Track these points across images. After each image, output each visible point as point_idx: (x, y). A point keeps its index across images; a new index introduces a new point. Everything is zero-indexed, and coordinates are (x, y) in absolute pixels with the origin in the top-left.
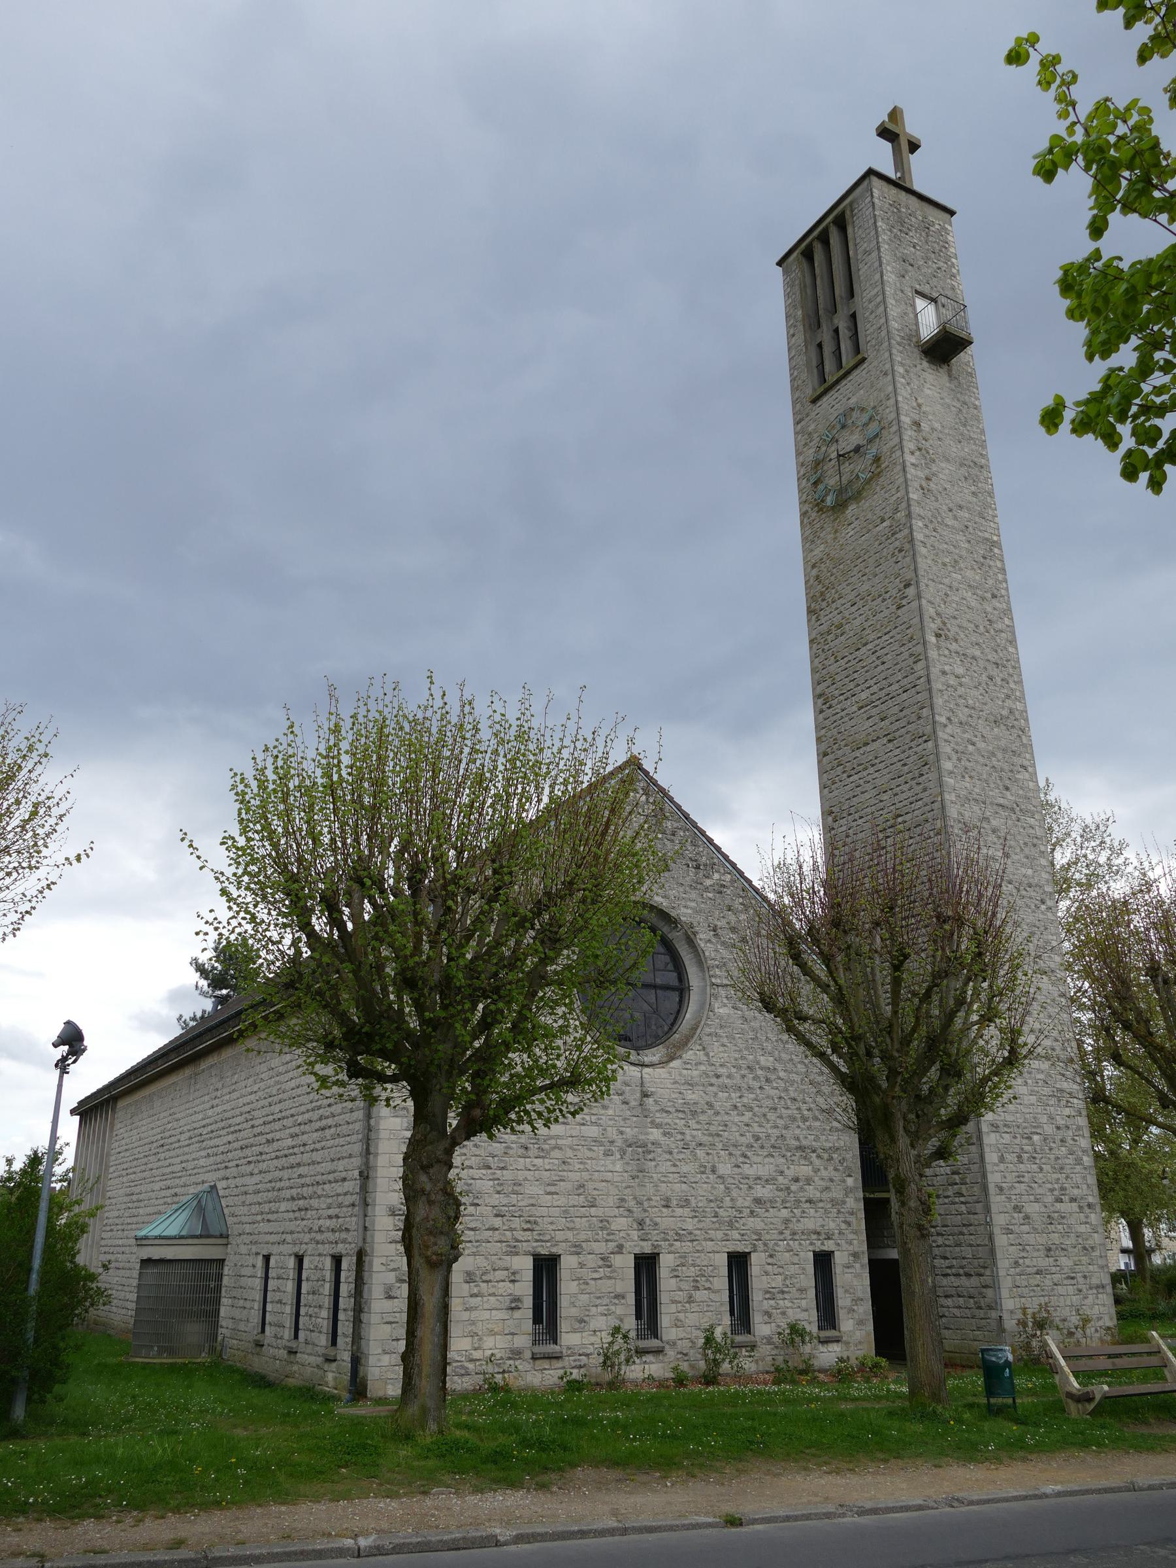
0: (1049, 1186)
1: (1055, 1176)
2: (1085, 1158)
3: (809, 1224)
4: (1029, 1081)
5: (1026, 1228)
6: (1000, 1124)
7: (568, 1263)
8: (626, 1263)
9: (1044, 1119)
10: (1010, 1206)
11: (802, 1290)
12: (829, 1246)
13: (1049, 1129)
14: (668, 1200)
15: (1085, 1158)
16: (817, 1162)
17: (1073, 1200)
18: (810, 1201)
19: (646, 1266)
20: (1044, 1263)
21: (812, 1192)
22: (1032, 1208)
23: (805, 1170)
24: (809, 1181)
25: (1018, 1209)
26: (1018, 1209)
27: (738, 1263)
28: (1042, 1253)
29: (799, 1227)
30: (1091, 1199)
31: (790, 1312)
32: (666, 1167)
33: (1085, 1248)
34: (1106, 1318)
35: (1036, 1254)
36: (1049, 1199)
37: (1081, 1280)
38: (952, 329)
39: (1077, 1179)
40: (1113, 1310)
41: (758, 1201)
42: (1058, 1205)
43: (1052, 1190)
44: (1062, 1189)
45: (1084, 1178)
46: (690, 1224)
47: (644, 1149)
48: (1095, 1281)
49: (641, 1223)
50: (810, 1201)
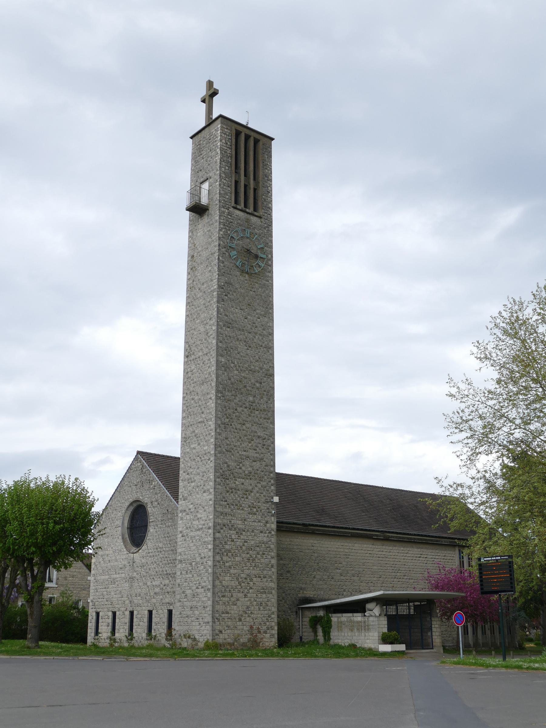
0: (195, 582)
1: (198, 578)
2: (210, 570)
3: (167, 600)
4: (194, 541)
5: (185, 600)
6: (182, 560)
7: (117, 613)
8: (127, 613)
9: (197, 555)
10: (181, 591)
11: (164, 623)
12: (171, 608)
13: (198, 559)
14: (136, 594)
15: (210, 570)
16: (171, 578)
17: (202, 587)
18: (168, 593)
19: (132, 613)
20: (190, 613)
21: (169, 589)
22: (189, 592)
23: (167, 582)
24: (168, 585)
25: (183, 592)
26: (183, 592)
27: (150, 612)
28: (189, 609)
29: (164, 601)
30: (209, 587)
31: (160, 630)
32: (136, 584)
33: (204, 607)
34: (208, 635)
35: (187, 610)
36: (194, 588)
37: (201, 620)
38: (197, 216)
39: (205, 579)
40: (211, 633)
41: (155, 593)
42: (197, 590)
43: (195, 584)
44: (199, 583)
45: (208, 578)
46: (141, 602)
47: (132, 578)
48: (206, 620)
49: (131, 602)
50: (168, 593)
